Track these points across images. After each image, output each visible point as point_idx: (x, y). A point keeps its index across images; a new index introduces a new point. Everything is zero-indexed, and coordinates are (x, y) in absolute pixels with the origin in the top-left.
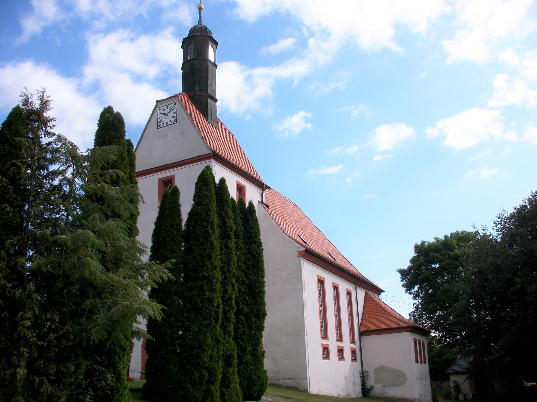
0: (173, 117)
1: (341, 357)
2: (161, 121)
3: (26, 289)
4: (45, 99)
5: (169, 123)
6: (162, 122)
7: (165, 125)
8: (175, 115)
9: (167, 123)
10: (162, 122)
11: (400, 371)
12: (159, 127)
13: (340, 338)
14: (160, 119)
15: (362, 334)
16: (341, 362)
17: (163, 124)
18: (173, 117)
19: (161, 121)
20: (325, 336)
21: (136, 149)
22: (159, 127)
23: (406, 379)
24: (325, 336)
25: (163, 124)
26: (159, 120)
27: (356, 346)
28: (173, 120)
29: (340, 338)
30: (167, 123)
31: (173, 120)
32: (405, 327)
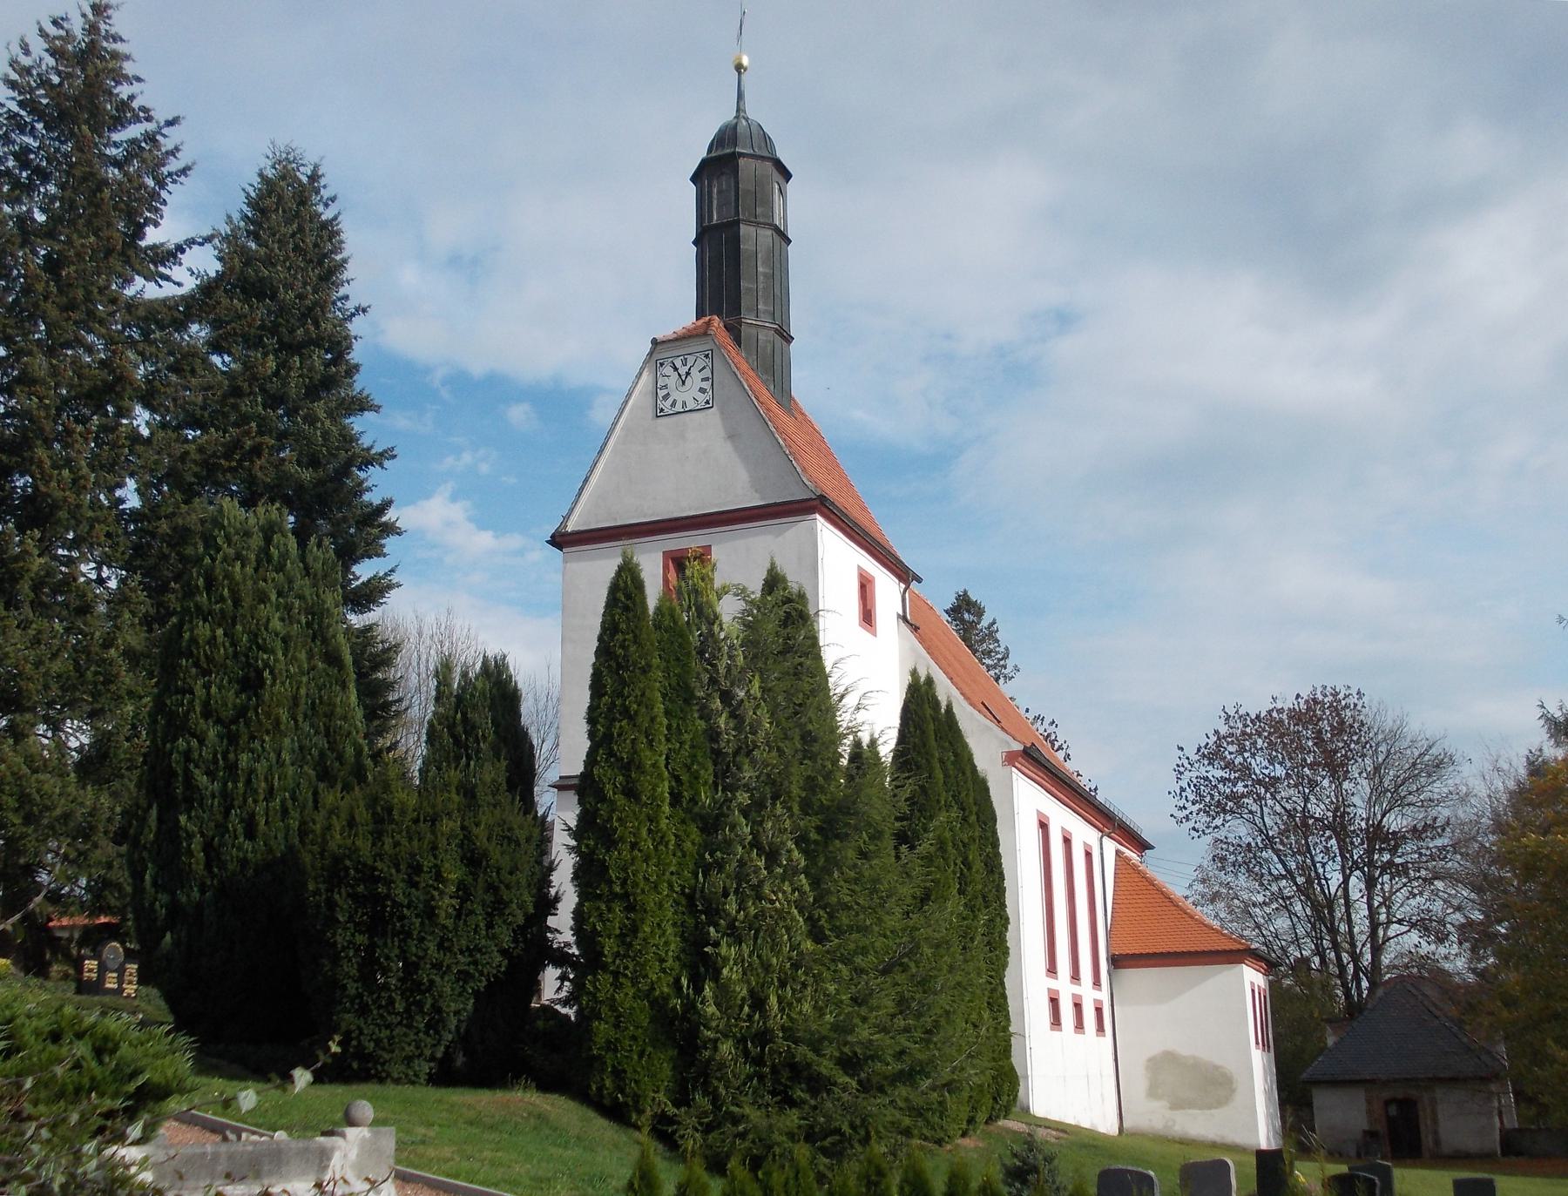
0: (702, 390)
1: (1079, 1026)
2: (666, 397)
3: (694, 820)
4: (387, 463)
5: (691, 405)
6: (670, 401)
7: (679, 408)
8: (707, 385)
9: (684, 404)
10: (670, 401)
11: (1216, 1068)
12: (659, 414)
13: (1076, 976)
14: (664, 392)
15: (1116, 962)
16: (1080, 1036)
17: (674, 404)
18: (702, 390)
19: (666, 397)
20: (1052, 970)
21: (640, 374)
22: (659, 414)
23: (1233, 1091)
24: (1052, 970)
25: (674, 404)
26: (661, 393)
27: (1104, 995)
28: (702, 398)
29: (1076, 976)
30: (684, 404)
31: (702, 398)
32: (1225, 951)
